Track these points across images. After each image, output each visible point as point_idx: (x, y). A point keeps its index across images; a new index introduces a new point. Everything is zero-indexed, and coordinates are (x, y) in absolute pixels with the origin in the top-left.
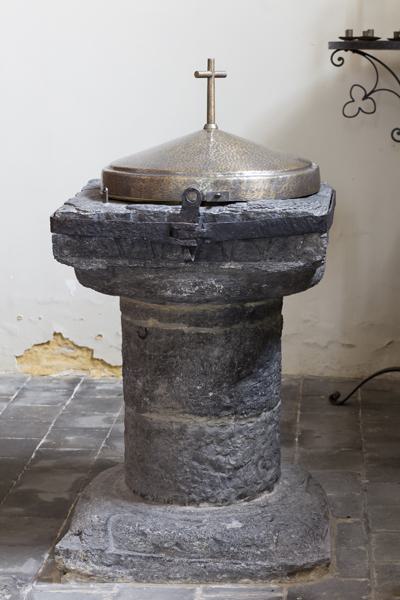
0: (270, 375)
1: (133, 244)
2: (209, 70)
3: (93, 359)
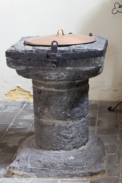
0: (84, 106)
1: (34, 61)
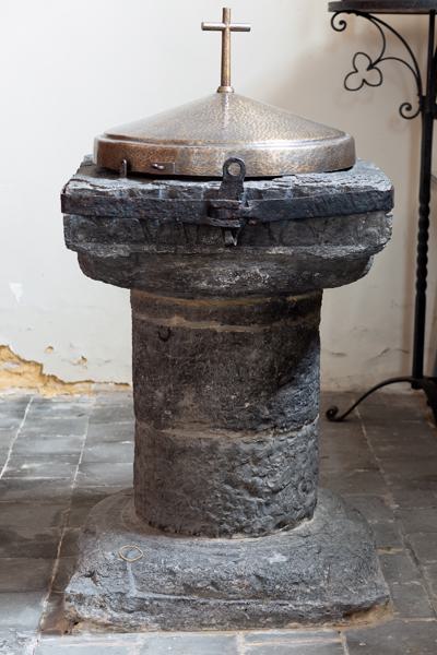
1: (162, 225)
2: (224, 22)
3: (42, 375)
